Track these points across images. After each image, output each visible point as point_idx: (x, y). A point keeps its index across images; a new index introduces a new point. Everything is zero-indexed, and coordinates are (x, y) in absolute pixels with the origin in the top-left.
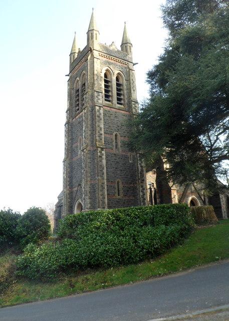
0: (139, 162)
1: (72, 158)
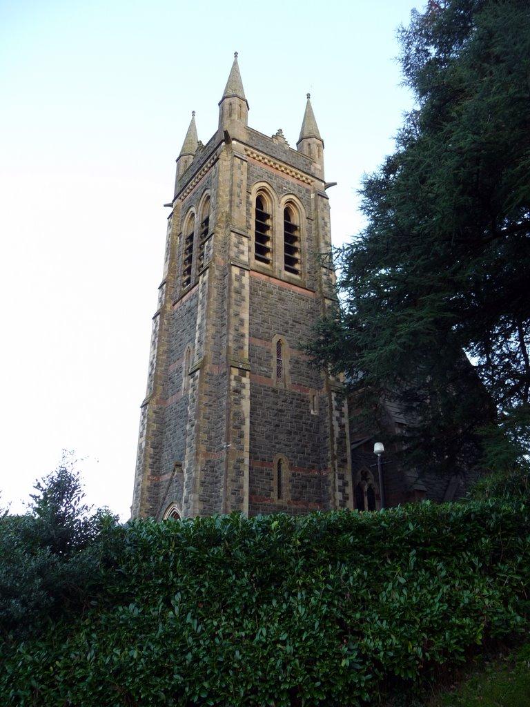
0: (336, 414)
1: (164, 399)
